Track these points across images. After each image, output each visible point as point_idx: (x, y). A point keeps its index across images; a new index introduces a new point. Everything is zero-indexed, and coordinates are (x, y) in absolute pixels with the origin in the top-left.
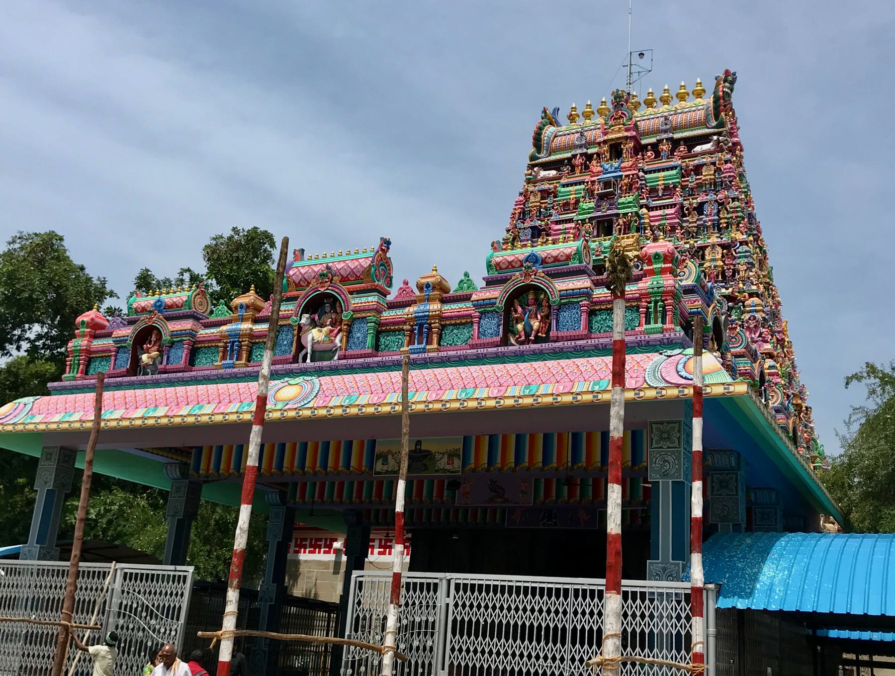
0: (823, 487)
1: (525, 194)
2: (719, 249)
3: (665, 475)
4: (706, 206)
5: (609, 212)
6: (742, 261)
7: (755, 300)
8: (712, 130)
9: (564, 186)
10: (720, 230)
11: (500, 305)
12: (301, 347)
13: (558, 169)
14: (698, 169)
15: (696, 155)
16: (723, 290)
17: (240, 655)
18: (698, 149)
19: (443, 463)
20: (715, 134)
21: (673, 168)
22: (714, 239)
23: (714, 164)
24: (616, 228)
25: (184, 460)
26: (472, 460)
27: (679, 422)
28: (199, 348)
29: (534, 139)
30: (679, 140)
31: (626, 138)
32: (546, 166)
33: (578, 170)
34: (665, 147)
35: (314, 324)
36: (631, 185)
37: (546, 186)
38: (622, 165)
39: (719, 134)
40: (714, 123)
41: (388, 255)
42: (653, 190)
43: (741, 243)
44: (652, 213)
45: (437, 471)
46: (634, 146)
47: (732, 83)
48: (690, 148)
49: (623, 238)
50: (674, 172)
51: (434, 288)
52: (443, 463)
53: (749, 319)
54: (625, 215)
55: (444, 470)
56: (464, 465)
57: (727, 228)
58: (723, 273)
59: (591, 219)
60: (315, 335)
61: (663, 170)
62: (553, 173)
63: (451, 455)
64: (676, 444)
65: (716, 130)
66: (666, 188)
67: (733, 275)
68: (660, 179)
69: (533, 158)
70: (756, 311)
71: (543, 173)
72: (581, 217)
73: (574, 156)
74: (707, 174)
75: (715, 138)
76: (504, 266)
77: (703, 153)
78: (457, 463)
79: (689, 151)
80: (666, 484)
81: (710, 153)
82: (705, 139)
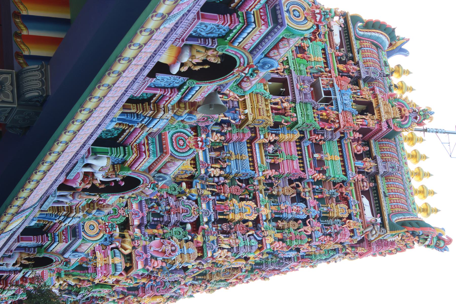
2: (254, 217)
4: (302, 205)
5: (297, 92)
8: (386, 217)
13: (341, 46)
16: (206, 220)
18: (365, 201)
20: (382, 220)
23: (350, 217)
24: (278, 99)
28: (219, 163)
32: (345, 32)
33: (341, 67)
34: (368, 164)
36: (327, 121)
39: (383, 225)
42: (318, 148)
43: (260, 242)
44: (293, 145)
46: (369, 130)
47: (437, 247)
48: (366, 193)
49: (267, 105)
53: (173, 245)
57: (278, 228)
58: (225, 221)
62: (337, 40)
65: (387, 222)
66: (321, 162)
67: (223, 232)
68: (331, 154)
69: (356, 19)
71: (336, 30)
73: (357, 64)
74: (340, 210)
75: (379, 220)
81: (362, 215)
82: (377, 209)
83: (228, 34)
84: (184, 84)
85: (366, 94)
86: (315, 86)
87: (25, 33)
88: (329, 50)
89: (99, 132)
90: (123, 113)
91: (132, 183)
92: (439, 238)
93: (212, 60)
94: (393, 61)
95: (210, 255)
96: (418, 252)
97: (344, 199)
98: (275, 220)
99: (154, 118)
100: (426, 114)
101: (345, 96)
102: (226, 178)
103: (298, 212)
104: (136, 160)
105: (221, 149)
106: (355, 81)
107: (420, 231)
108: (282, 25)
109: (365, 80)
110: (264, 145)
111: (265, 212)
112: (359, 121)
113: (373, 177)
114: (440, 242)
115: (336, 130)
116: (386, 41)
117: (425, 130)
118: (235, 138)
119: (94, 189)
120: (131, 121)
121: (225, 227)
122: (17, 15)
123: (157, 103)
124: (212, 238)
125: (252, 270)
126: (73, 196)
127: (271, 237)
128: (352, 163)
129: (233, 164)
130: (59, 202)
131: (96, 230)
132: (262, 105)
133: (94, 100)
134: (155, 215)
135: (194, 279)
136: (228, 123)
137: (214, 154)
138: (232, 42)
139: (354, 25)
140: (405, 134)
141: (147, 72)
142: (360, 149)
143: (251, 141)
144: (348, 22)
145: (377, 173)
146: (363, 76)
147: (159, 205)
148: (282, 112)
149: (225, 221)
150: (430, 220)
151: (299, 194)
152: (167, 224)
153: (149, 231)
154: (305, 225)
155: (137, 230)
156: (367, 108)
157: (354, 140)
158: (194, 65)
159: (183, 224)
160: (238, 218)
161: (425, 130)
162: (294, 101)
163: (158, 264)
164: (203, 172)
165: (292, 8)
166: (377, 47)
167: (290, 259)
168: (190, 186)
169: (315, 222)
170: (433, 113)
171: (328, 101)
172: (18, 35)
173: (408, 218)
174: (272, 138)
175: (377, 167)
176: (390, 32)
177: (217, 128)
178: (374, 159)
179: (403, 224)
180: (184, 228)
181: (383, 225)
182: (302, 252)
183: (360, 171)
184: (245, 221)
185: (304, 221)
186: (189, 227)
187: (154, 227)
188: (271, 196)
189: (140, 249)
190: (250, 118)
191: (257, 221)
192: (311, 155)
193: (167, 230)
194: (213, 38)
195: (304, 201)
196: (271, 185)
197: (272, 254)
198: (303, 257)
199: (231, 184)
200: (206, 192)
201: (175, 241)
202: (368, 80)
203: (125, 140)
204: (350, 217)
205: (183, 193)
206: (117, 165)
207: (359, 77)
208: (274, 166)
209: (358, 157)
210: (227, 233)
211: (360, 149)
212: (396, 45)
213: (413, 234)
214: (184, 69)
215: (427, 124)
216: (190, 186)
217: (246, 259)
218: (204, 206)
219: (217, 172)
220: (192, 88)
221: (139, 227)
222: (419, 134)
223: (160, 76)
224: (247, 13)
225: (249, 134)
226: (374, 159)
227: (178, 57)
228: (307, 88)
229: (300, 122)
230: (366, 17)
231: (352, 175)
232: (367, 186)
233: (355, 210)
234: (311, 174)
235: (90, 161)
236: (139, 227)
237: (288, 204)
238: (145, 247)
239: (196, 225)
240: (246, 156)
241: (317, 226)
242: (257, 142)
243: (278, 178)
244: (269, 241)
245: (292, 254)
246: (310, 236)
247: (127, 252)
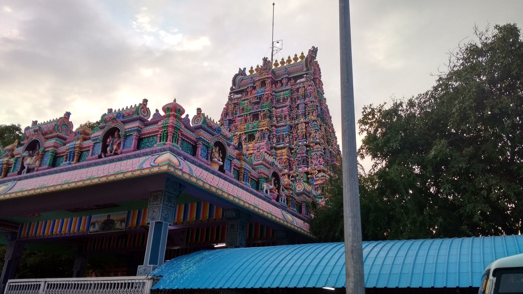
2: (304, 124)
3: (153, 219)
5: (257, 110)
6: (313, 129)
7: (318, 146)
9: (243, 101)
11: (101, 138)
12: (23, 167)
13: (242, 94)
16: (305, 142)
18: (298, 81)
19: (118, 226)
21: (287, 90)
23: (304, 87)
24: (260, 117)
25: (14, 230)
26: (130, 223)
27: (162, 191)
29: (233, 81)
30: (291, 78)
31: (267, 78)
32: (237, 93)
33: (249, 94)
34: (284, 81)
35: (31, 156)
37: (236, 101)
39: (307, 74)
41: (70, 120)
43: (313, 121)
44: (277, 110)
45: (115, 230)
46: (272, 81)
48: (296, 81)
50: (287, 92)
51: (81, 134)
52: (118, 226)
54: (264, 111)
55: (118, 229)
56: (126, 226)
57: (308, 114)
58: (306, 135)
59: (250, 114)
60: (29, 161)
62: (239, 96)
63: (122, 221)
64: (165, 203)
67: (310, 135)
69: (232, 89)
70: (318, 151)
73: (248, 88)
74: (301, 91)
75: (305, 76)
76: (108, 120)
77: (300, 83)
78: (124, 225)
80: (152, 223)
81: (303, 82)
82: (301, 77)
83: (206, 145)
85: (258, 84)
86: (256, 103)
90: (243, 181)
91: (275, 175)
92: (313, 51)
95: (318, 140)
96: (319, 58)
97: (298, 90)
98: (305, 116)
99: (245, 169)
100: (265, 60)
101: (259, 91)
102: (290, 135)
103: (302, 107)
106: (254, 88)
108: (201, 126)
110: (278, 122)
111: (302, 120)
113: (289, 79)
114: (314, 51)
117: (272, 60)
118: (275, 133)
119: (278, 189)
120: (247, 177)
121: (308, 135)
122: (208, 220)
123: (239, 168)
124: (312, 140)
126: (281, 196)
128: (284, 88)
129: (284, 133)
130: (284, 201)
131: (300, 186)
133: (223, 194)
134: (303, 162)
135: (329, 145)
136: (269, 136)
137: (281, 141)
138: (209, 144)
142: (279, 84)
143: (276, 127)
144: (233, 91)
145: (287, 77)
146: (252, 85)
148: (265, 115)
149: (306, 135)
150: (306, 54)
152: (307, 157)
153: (310, 164)
154: (307, 104)
155: (309, 168)
156: (263, 83)
157: (276, 87)
158: (220, 156)
159: (307, 151)
160: (304, 130)
162: (260, 111)
163: (321, 159)
164: (287, 144)
165: (196, 122)
166: (242, 80)
167: (321, 109)
168: (293, 149)
169: (306, 101)
171: (260, 98)
172: (215, 219)
173: (304, 64)
174: (275, 119)
176: (236, 76)
177: (271, 140)
178: (283, 79)
179: (307, 66)
181: (307, 74)
182: (318, 104)
183: (287, 84)
184: (306, 127)
187: (308, 162)
188: (297, 118)
189: (316, 167)
190: (267, 127)
191: (306, 123)
193: (309, 157)
194: (208, 150)
195: (298, 105)
196: (293, 118)
197: (318, 116)
199: (292, 133)
200: (295, 142)
201: (313, 154)
202: (254, 83)
203: (256, 178)
204: (304, 87)
205: (296, 151)
206: (267, 180)
207: (252, 86)
208: (285, 118)
210: (310, 134)
211: (279, 84)
212: (242, 72)
213: (311, 62)
214: (221, 160)
215: (269, 59)
216: (293, 149)
217: (321, 126)
218: (300, 143)
219: (288, 138)
221: (308, 168)
223: (225, 168)
224: (197, 139)
225: (274, 128)
226: (283, 79)
227: (216, 163)
228: (256, 106)
229: (268, 108)
231: (289, 87)
232: (292, 81)
234: (288, 103)
235: (264, 191)
236: (308, 168)
237: (299, 111)
238: (315, 165)
239: (307, 146)
240: (282, 128)
241: (307, 99)
242: (277, 124)
243: (290, 116)
244: (313, 118)
245: (319, 108)
246: (311, 102)
247: (317, 172)
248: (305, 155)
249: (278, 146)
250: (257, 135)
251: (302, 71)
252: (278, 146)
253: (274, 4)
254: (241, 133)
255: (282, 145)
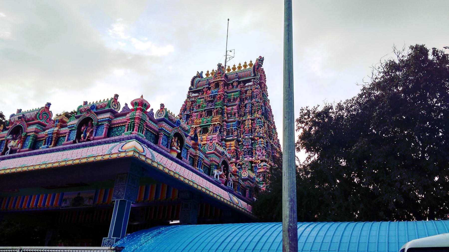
0: (253, 216)
1: (186, 102)
2: (250, 121)
3: (118, 198)
5: (211, 107)
6: (258, 125)
7: (262, 140)
9: (199, 99)
10: (252, 114)
12: (6, 149)
14: (246, 91)
15: (246, 87)
17: (381, 214)
18: (247, 84)
21: (237, 91)
22: (249, 117)
23: (251, 90)
31: (221, 81)
32: (195, 92)
33: (205, 93)
34: (235, 84)
35: (14, 139)
37: (193, 99)
38: (219, 90)
39: (254, 79)
40: (253, 75)
44: (228, 108)
45: (84, 206)
46: (224, 84)
47: (262, 61)
55: (86, 205)
57: (254, 113)
58: (251, 130)
59: (205, 110)
60: (12, 143)
61: (234, 92)
62: (197, 94)
63: (90, 198)
67: (255, 131)
69: (190, 89)
71: (194, 95)
72: (202, 109)
73: (204, 88)
77: (248, 86)
78: (92, 202)
79: (244, 85)
81: (251, 86)
82: (249, 81)
84: (185, 148)
86: (210, 101)
87: (171, 198)
88: (199, 97)
89: (205, 175)
92: (260, 60)
93: (176, 140)
94: (204, 76)
95: (262, 135)
96: (265, 66)
97: (246, 91)
98: (252, 114)
99: (199, 157)
100: (219, 65)
103: (249, 106)
104: (215, 162)
105: (229, 131)
106: (209, 89)
107: (256, 67)
109: (209, 85)
111: (249, 117)
112: (221, 88)
113: (239, 83)
114: (261, 60)
115: (223, 95)
116: (198, 79)
117: (225, 66)
119: (227, 175)
120: (200, 164)
124: (256, 134)
125: (269, 121)
127: (257, 115)
128: (235, 90)
129: (233, 128)
131: (245, 173)
132: (214, 119)
133: (180, 178)
134: (249, 152)
135: (271, 139)
137: (230, 134)
138: (169, 134)
139: (192, 89)
140: (226, 72)
141: (180, 160)
143: (227, 122)
144: (191, 91)
147: (245, 151)
151: (244, 106)
155: (253, 158)
156: (217, 85)
157: (228, 88)
161: (225, 66)
162: (214, 108)
164: (236, 137)
166: (199, 81)
169: (253, 101)
170: (260, 57)
173: (252, 71)
175: (236, 81)
179: (254, 72)
180: (253, 143)
181: (254, 79)
182: (262, 104)
183: (237, 87)
185: (252, 104)
186: (253, 142)
188: (244, 115)
189: (259, 157)
190: (219, 122)
191: (252, 120)
192: (232, 103)
194: (168, 140)
196: (241, 115)
197: (262, 114)
198: (265, 104)
200: (242, 136)
201: (257, 146)
202: (209, 84)
204: (251, 90)
205: (242, 144)
206: (217, 167)
208: (235, 115)
209: (233, 87)
212: (200, 75)
214: (179, 148)
215: (223, 65)
216: (240, 141)
217: (264, 123)
218: (246, 137)
220: (186, 145)
222: (227, 68)
223: (182, 156)
225: (225, 123)
227: (175, 151)
228: (210, 104)
229: (220, 106)
230: (190, 85)
231: (238, 89)
233: (249, 88)
234: (237, 102)
238: (258, 156)
239: (252, 139)
240: (231, 124)
241: (254, 100)
244: (258, 116)
246: (257, 102)
248: (250, 147)
249: (227, 138)
250: (210, 128)
251: (250, 76)
252: (227, 138)
253: (228, 20)
254: (197, 126)
255: (231, 138)
